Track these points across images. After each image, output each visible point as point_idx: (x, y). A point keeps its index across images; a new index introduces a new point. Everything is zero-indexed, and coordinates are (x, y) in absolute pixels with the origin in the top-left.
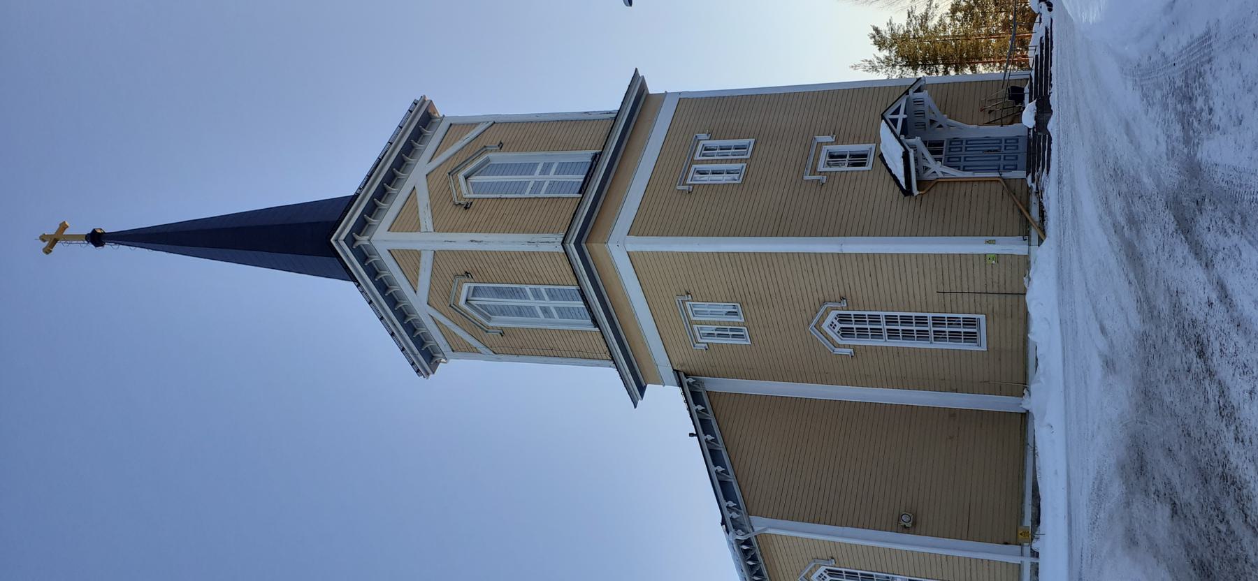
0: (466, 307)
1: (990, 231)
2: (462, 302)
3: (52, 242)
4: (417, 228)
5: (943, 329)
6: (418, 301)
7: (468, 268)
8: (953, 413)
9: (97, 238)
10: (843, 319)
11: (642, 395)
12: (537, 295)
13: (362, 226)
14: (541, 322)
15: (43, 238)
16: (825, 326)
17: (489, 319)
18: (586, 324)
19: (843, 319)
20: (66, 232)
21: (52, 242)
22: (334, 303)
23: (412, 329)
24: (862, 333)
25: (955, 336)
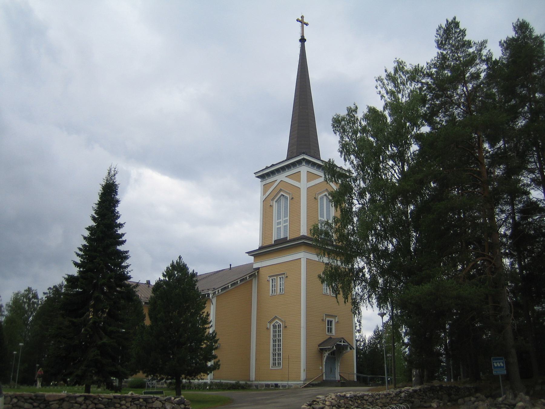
0: (280, 194)
1: (307, 370)
2: (282, 193)
3: (302, 22)
4: (308, 180)
5: (277, 354)
6: (282, 177)
7: (295, 199)
8: (249, 359)
9: (303, 40)
10: (279, 326)
11: (257, 177)
12: (285, 221)
13: (308, 162)
14: (275, 221)
15: (302, 17)
16: (277, 320)
17: (276, 202)
18: (275, 238)
19: (279, 326)
20: (305, 25)
21: (302, 22)
22: (278, 148)
23: (273, 173)
24: (275, 332)
25: (274, 360)
